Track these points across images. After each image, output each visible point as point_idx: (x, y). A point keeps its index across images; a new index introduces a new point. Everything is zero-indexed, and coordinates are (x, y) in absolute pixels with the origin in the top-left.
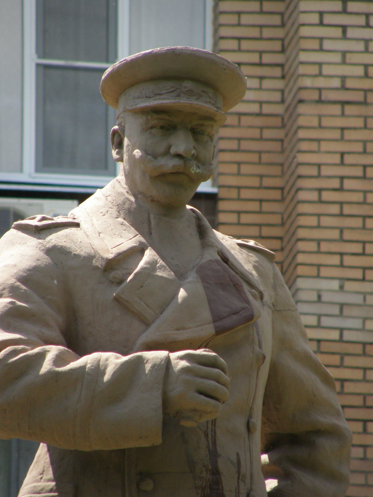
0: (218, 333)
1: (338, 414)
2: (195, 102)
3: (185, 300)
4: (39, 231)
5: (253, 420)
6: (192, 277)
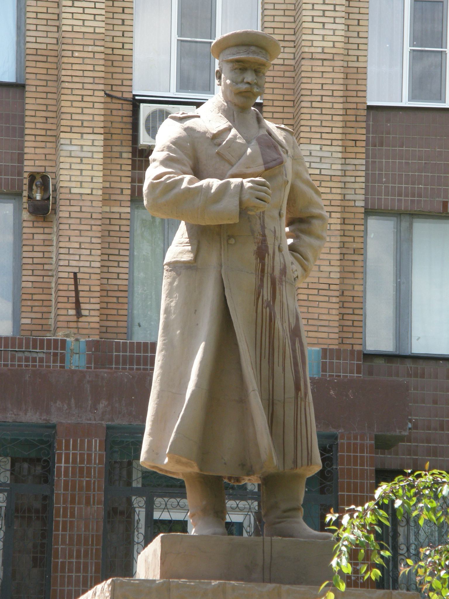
1: (322, 208)
2: (256, 57)
3: (250, 154)
4: (181, 120)
6: (254, 142)
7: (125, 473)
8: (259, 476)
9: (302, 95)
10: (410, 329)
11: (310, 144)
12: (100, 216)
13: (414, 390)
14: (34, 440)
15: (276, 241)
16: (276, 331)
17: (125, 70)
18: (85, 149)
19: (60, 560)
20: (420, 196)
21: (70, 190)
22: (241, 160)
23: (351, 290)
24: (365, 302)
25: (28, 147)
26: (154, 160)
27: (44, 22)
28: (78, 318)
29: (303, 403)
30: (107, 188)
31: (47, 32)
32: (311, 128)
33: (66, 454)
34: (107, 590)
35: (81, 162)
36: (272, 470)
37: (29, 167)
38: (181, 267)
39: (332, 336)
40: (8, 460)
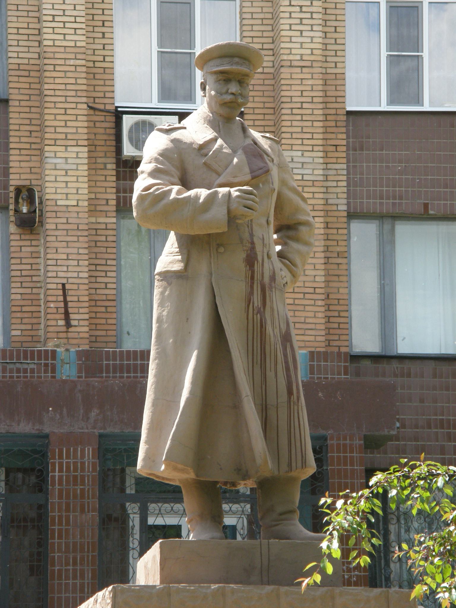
0: (253, 179)
3: (237, 163)
5: (270, 219)
6: (240, 152)
7: (118, 480)
8: (255, 480)
9: (282, 102)
10: (395, 329)
11: (292, 150)
12: (86, 227)
13: (401, 389)
14: (27, 450)
15: (265, 249)
16: (267, 337)
17: (107, 83)
18: (70, 161)
19: (57, 568)
20: (401, 198)
21: (56, 202)
22: (228, 170)
23: (336, 293)
24: (351, 304)
25: (14, 161)
26: (142, 172)
27: (26, 37)
28: (68, 328)
29: (296, 407)
30: (93, 199)
31: (29, 47)
32: (292, 135)
33: (59, 463)
34: (108, 596)
35: (66, 175)
36: (267, 474)
37: (15, 180)
38: (172, 276)
39: (319, 339)
40: (2, 470)
